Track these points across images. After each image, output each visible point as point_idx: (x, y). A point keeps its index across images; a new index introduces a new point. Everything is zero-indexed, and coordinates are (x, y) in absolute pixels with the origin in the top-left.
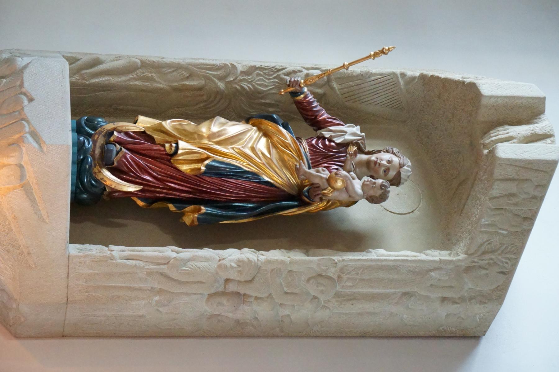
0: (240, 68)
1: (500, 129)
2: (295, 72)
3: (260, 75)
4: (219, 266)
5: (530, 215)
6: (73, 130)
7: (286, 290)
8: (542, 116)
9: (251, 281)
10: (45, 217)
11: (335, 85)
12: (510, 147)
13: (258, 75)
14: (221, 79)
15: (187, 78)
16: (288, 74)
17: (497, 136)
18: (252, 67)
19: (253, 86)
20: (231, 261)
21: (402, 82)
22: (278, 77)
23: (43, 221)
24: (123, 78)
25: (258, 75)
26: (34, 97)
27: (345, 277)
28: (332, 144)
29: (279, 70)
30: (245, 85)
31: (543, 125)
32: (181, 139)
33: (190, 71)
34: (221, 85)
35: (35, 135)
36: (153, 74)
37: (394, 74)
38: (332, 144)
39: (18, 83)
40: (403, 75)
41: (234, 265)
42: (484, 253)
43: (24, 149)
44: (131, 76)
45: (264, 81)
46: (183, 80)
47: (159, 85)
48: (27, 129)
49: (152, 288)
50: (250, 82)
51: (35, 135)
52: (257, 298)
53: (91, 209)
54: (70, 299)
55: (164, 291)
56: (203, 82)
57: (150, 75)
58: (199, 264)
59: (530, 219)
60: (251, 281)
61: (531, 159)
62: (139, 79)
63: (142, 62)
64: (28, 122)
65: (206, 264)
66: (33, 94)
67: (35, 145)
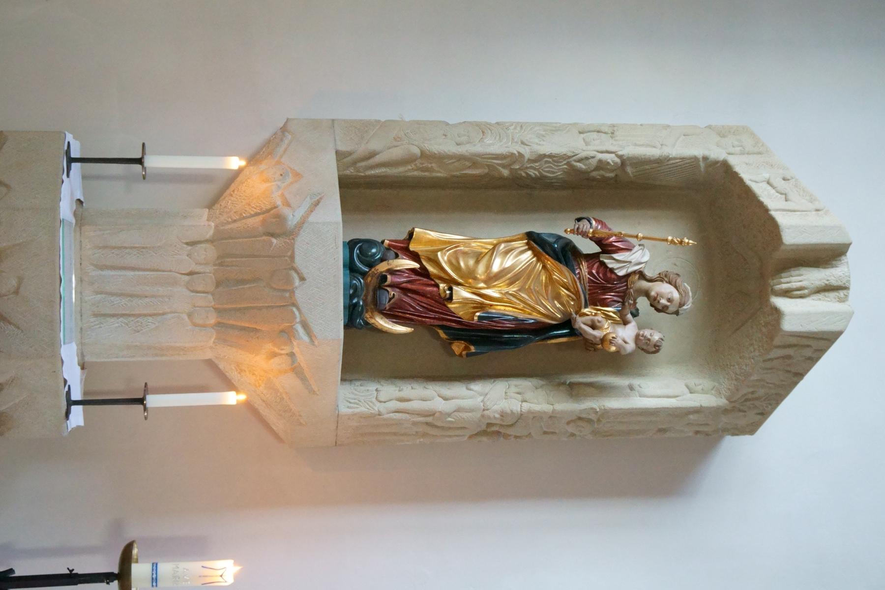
0: (527, 156)
1: (794, 272)
2: (587, 158)
3: (549, 162)
4: (483, 416)
5: (801, 371)
6: (344, 266)
7: (545, 430)
8: (843, 257)
9: (512, 425)
10: (316, 389)
11: (629, 170)
12: (797, 313)
13: (547, 162)
14: (504, 166)
15: (469, 167)
16: (580, 161)
17: (788, 283)
18: (541, 155)
19: (540, 172)
20: (496, 412)
21: (702, 164)
22: (568, 164)
23: (314, 393)
24: (401, 169)
25: (547, 162)
26: (305, 276)
27: (604, 421)
28: (613, 276)
29: (570, 157)
30: (532, 173)
31: (840, 274)
32: (458, 284)
33: (473, 160)
34: (506, 172)
35: (305, 326)
36: (433, 165)
37: (696, 159)
38: (613, 276)
39: (289, 254)
40: (705, 158)
41: (497, 416)
42: (746, 400)
43: (295, 343)
44: (410, 167)
45: (551, 167)
46: (463, 170)
47: (439, 175)
48: (298, 320)
49: (417, 432)
50: (535, 169)
51: (305, 326)
52: (516, 437)
53: (363, 356)
54: (339, 443)
55: (427, 434)
56: (486, 171)
57: (430, 166)
58: (464, 415)
59: (800, 375)
60: (512, 425)
61: (816, 330)
62: (418, 169)
63: (422, 153)
64: (298, 309)
65: (470, 414)
66: (304, 272)
67: (306, 338)
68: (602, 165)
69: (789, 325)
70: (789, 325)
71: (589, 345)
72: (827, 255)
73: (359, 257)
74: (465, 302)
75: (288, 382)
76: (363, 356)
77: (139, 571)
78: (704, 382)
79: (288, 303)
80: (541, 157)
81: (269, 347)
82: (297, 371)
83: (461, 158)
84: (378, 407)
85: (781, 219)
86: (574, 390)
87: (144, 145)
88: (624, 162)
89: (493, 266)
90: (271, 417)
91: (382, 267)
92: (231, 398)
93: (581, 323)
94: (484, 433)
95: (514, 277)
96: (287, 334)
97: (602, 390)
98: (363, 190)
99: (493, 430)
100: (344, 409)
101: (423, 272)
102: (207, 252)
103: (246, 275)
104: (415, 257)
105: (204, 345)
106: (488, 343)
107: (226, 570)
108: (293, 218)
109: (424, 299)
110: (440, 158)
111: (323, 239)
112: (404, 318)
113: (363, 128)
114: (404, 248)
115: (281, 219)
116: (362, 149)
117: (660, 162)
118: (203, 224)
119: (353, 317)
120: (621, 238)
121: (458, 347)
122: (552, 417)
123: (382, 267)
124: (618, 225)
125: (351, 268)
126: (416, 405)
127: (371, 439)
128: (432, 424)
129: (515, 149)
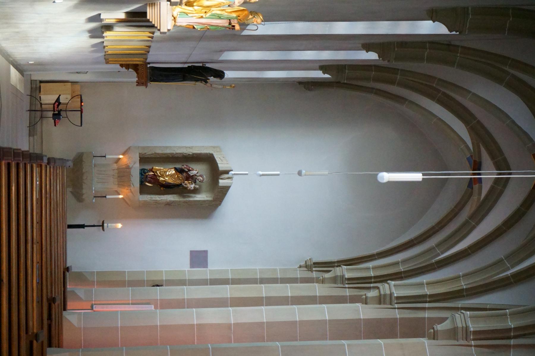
12: (222, 182)
53: (143, 190)
68: (189, 154)
69: (220, 185)
70: (220, 185)
71: (186, 188)
72: (227, 172)
73: (143, 172)
74: (162, 181)
75: (130, 194)
76: (143, 190)
77: (105, 225)
78: (208, 195)
79: (130, 180)
80: (177, 153)
81: (127, 188)
82: (132, 192)
83: (162, 154)
84: (147, 199)
85: (219, 165)
86: (184, 197)
87: (55, 126)
88: (193, 154)
89: (168, 174)
90: (127, 200)
91: (147, 174)
92: (121, 196)
93: (183, 184)
94: (167, 204)
95: (171, 176)
96: (130, 186)
97: (189, 197)
98: (143, 159)
99: (169, 204)
100: (140, 199)
101: (154, 175)
102: (116, 171)
103: (123, 175)
104: (153, 172)
105: (116, 188)
106: (168, 188)
107: (119, 226)
108: (131, 166)
109: (155, 179)
110: (158, 154)
111: (136, 168)
112: (150, 183)
113: (144, 148)
114: (151, 170)
115: (128, 166)
116: (143, 153)
117: (200, 154)
118: (115, 166)
119: (142, 183)
120: (192, 169)
121: (162, 188)
122: (180, 201)
123: (147, 174)
124: (192, 166)
125: (141, 174)
126: (154, 199)
127: (145, 206)
128: (156, 202)
129: (172, 152)
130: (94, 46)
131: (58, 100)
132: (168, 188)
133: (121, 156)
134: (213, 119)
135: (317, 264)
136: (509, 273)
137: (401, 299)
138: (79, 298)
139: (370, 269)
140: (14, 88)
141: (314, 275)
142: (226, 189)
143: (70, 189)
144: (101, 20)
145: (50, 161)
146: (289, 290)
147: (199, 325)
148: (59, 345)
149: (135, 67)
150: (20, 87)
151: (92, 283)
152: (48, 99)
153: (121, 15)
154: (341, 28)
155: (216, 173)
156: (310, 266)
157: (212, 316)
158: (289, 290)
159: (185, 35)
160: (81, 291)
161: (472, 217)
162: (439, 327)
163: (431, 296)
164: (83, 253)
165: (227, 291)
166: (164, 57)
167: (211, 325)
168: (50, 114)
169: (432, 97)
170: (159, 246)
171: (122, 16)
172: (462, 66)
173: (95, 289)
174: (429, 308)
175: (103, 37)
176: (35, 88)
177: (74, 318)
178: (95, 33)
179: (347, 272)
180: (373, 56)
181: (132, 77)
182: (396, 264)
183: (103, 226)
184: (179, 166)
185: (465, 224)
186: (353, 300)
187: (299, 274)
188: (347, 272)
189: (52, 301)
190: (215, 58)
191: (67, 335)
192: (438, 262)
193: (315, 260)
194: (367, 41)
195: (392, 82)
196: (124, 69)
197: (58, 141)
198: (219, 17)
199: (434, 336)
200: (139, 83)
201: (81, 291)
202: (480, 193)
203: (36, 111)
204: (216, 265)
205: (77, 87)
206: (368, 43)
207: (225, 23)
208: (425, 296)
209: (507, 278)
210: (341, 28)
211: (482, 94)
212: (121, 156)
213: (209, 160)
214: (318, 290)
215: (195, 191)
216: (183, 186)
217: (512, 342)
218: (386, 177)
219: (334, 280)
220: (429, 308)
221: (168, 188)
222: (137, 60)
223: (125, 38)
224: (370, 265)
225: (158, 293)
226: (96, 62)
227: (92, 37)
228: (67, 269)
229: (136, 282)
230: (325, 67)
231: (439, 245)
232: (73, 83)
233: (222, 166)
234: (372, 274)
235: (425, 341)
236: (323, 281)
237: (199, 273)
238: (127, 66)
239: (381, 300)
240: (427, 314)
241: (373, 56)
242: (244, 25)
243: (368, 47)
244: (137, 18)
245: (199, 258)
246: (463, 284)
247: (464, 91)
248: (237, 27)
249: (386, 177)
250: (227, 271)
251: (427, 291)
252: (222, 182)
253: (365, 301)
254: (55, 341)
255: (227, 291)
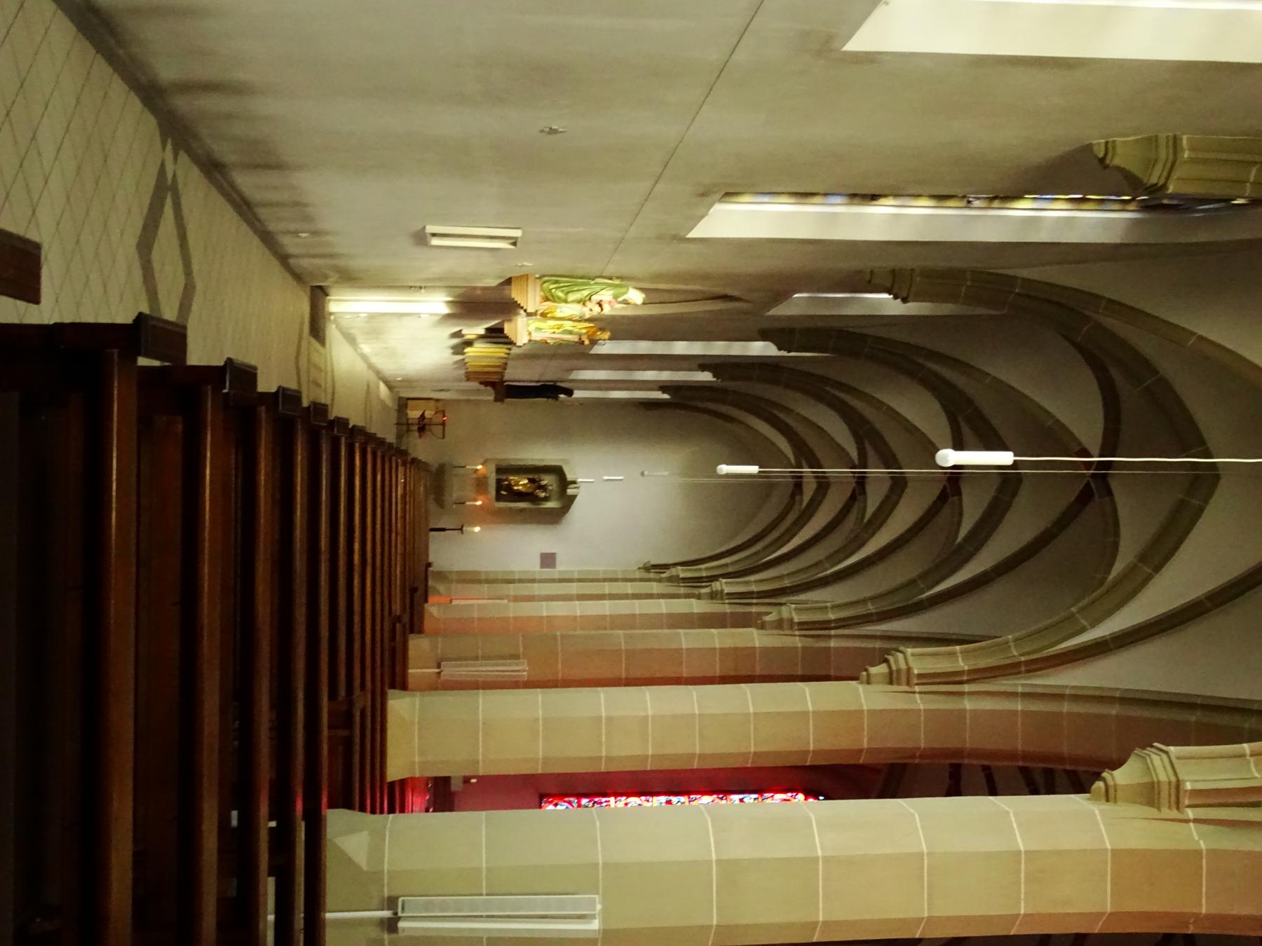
12: (570, 491)
53: (499, 498)
72: (574, 482)
73: (499, 481)
76: (499, 498)
89: (522, 483)
92: (479, 503)
98: (500, 470)
99: (522, 510)
103: (481, 484)
105: (472, 495)
107: (477, 529)
109: (509, 488)
124: (543, 476)
130: (456, 363)
131: (423, 416)
132: (520, 496)
133: (480, 467)
134: (562, 433)
135: (655, 566)
136: (829, 572)
137: (730, 595)
138: (438, 593)
139: (703, 570)
140: (382, 402)
141: (652, 575)
142: (573, 498)
143: (432, 496)
144: (463, 336)
145: (414, 461)
146: (629, 588)
147: (548, 617)
148: (421, 631)
149: (492, 384)
150: (389, 402)
151: (451, 581)
152: (414, 414)
153: (481, 330)
154: (680, 348)
155: (564, 483)
156: (648, 568)
157: (559, 609)
158: (629, 588)
159: (540, 352)
160: (441, 588)
161: (794, 524)
162: (767, 618)
163: (759, 592)
164: (445, 553)
165: (574, 588)
166: (519, 374)
167: (561, 618)
168: (415, 428)
169: (759, 416)
170: (512, 548)
171: (482, 332)
172: (787, 386)
173: (454, 586)
174: (756, 604)
175: (463, 354)
176: (403, 404)
177: (433, 609)
178: (458, 349)
179: (682, 572)
180: (706, 376)
181: (489, 395)
182: (726, 565)
183: (461, 529)
184: (531, 476)
185: (787, 530)
186: (687, 596)
187: (638, 575)
188: (682, 572)
189: (414, 590)
190: (565, 377)
191: (428, 624)
192: (768, 562)
193: (654, 562)
194: (700, 361)
195: (724, 402)
196: (482, 387)
197: (421, 448)
198: (570, 333)
199: (762, 626)
200: (496, 400)
201: (441, 588)
202: (801, 501)
203: (403, 425)
204: (562, 567)
205: (440, 404)
206: (704, 363)
207: (575, 338)
208: (752, 593)
209: (826, 577)
210: (680, 348)
211: (804, 413)
212: (480, 467)
213: (558, 471)
214: (655, 588)
215: (546, 499)
216: (536, 496)
217: (833, 632)
218: (724, 469)
219: (670, 579)
220: (756, 604)
221: (520, 496)
222: (494, 378)
223: (482, 352)
224: (703, 566)
225: (512, 589)
226: (459, 380)
227: (454, 353)
228: (429, 565)
229: (491, 581)
230: (664, 387)
231: (765, 548)
232: (437, 400)
233: (570, 477)
234: (704, 574)
235: (753, 630)
236: (660, 580)
237: (548, 573)
238: (486, 384)
239: (713, 596)
240: (754, 609)
241: (706, 376)
242: (594, 342)
243: (703, 367)
244: (496, 335)
245: (548, 560)
246: (787, 583)
247: (788, 411)
248: (587, 342)
249: (724, 469)
250: (572, 572)
251: (754, 588)
252: (570, 491)
253: (699, 597)
254: (416, 628)
255: (574, 588)
